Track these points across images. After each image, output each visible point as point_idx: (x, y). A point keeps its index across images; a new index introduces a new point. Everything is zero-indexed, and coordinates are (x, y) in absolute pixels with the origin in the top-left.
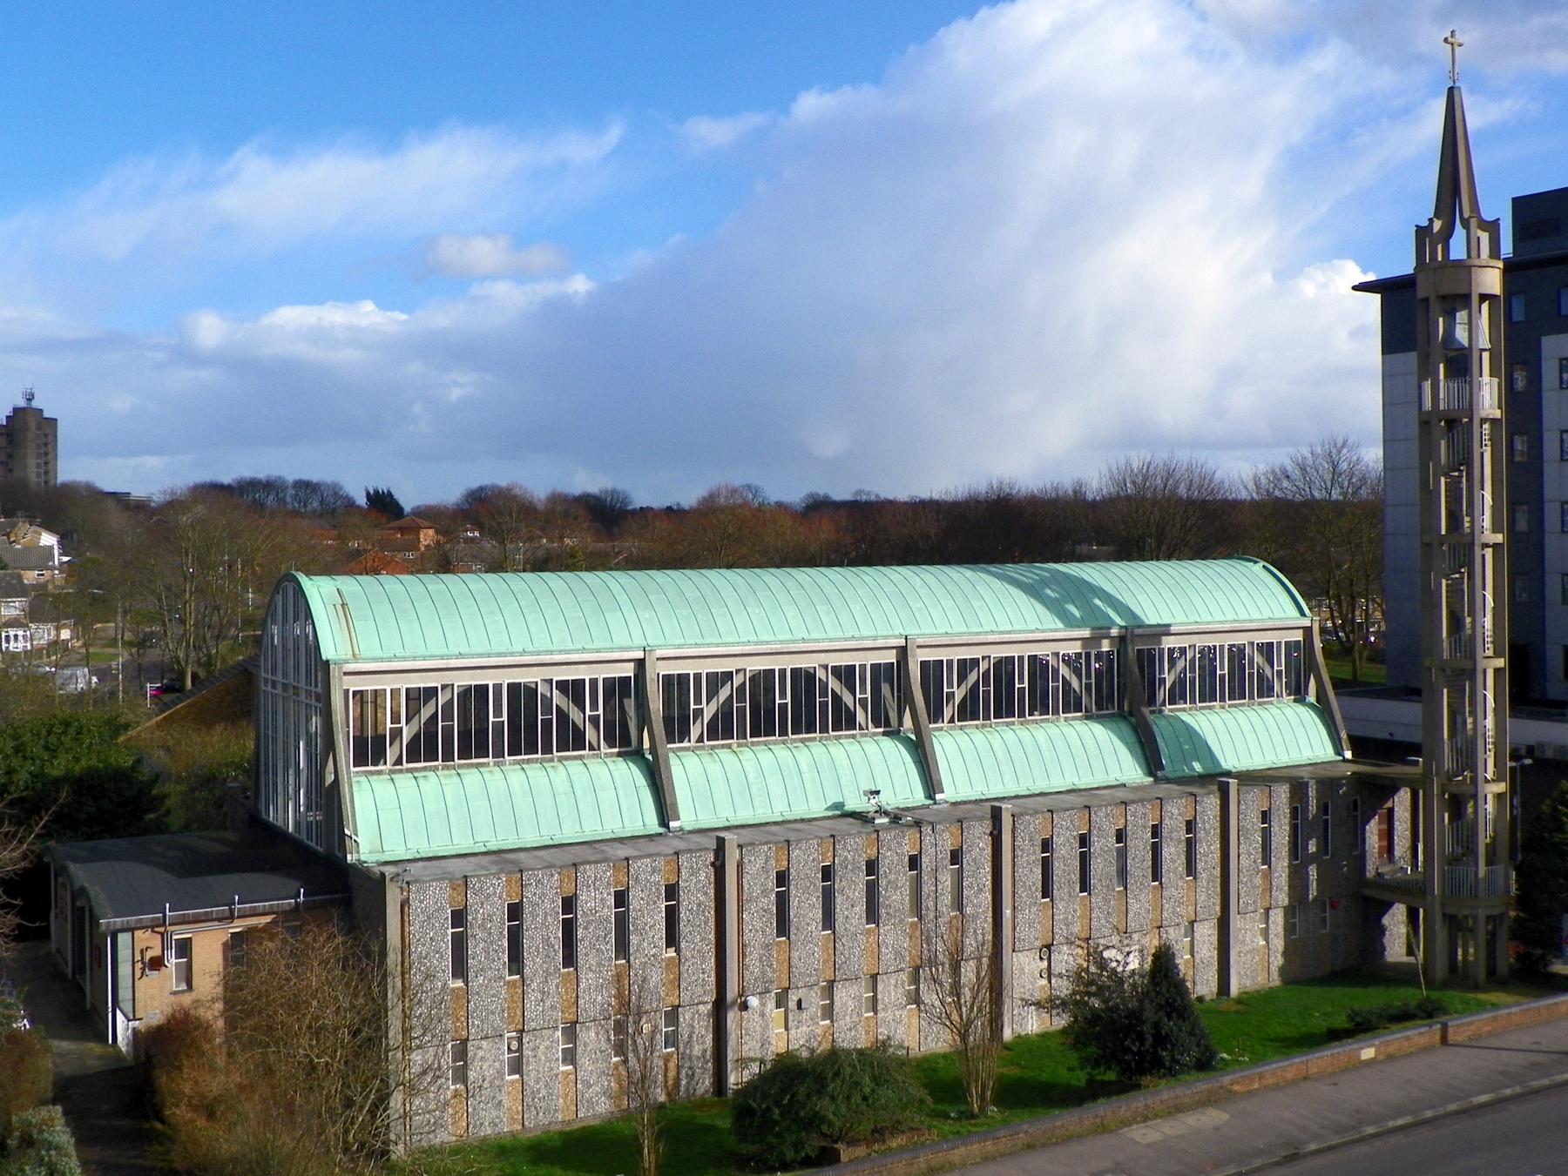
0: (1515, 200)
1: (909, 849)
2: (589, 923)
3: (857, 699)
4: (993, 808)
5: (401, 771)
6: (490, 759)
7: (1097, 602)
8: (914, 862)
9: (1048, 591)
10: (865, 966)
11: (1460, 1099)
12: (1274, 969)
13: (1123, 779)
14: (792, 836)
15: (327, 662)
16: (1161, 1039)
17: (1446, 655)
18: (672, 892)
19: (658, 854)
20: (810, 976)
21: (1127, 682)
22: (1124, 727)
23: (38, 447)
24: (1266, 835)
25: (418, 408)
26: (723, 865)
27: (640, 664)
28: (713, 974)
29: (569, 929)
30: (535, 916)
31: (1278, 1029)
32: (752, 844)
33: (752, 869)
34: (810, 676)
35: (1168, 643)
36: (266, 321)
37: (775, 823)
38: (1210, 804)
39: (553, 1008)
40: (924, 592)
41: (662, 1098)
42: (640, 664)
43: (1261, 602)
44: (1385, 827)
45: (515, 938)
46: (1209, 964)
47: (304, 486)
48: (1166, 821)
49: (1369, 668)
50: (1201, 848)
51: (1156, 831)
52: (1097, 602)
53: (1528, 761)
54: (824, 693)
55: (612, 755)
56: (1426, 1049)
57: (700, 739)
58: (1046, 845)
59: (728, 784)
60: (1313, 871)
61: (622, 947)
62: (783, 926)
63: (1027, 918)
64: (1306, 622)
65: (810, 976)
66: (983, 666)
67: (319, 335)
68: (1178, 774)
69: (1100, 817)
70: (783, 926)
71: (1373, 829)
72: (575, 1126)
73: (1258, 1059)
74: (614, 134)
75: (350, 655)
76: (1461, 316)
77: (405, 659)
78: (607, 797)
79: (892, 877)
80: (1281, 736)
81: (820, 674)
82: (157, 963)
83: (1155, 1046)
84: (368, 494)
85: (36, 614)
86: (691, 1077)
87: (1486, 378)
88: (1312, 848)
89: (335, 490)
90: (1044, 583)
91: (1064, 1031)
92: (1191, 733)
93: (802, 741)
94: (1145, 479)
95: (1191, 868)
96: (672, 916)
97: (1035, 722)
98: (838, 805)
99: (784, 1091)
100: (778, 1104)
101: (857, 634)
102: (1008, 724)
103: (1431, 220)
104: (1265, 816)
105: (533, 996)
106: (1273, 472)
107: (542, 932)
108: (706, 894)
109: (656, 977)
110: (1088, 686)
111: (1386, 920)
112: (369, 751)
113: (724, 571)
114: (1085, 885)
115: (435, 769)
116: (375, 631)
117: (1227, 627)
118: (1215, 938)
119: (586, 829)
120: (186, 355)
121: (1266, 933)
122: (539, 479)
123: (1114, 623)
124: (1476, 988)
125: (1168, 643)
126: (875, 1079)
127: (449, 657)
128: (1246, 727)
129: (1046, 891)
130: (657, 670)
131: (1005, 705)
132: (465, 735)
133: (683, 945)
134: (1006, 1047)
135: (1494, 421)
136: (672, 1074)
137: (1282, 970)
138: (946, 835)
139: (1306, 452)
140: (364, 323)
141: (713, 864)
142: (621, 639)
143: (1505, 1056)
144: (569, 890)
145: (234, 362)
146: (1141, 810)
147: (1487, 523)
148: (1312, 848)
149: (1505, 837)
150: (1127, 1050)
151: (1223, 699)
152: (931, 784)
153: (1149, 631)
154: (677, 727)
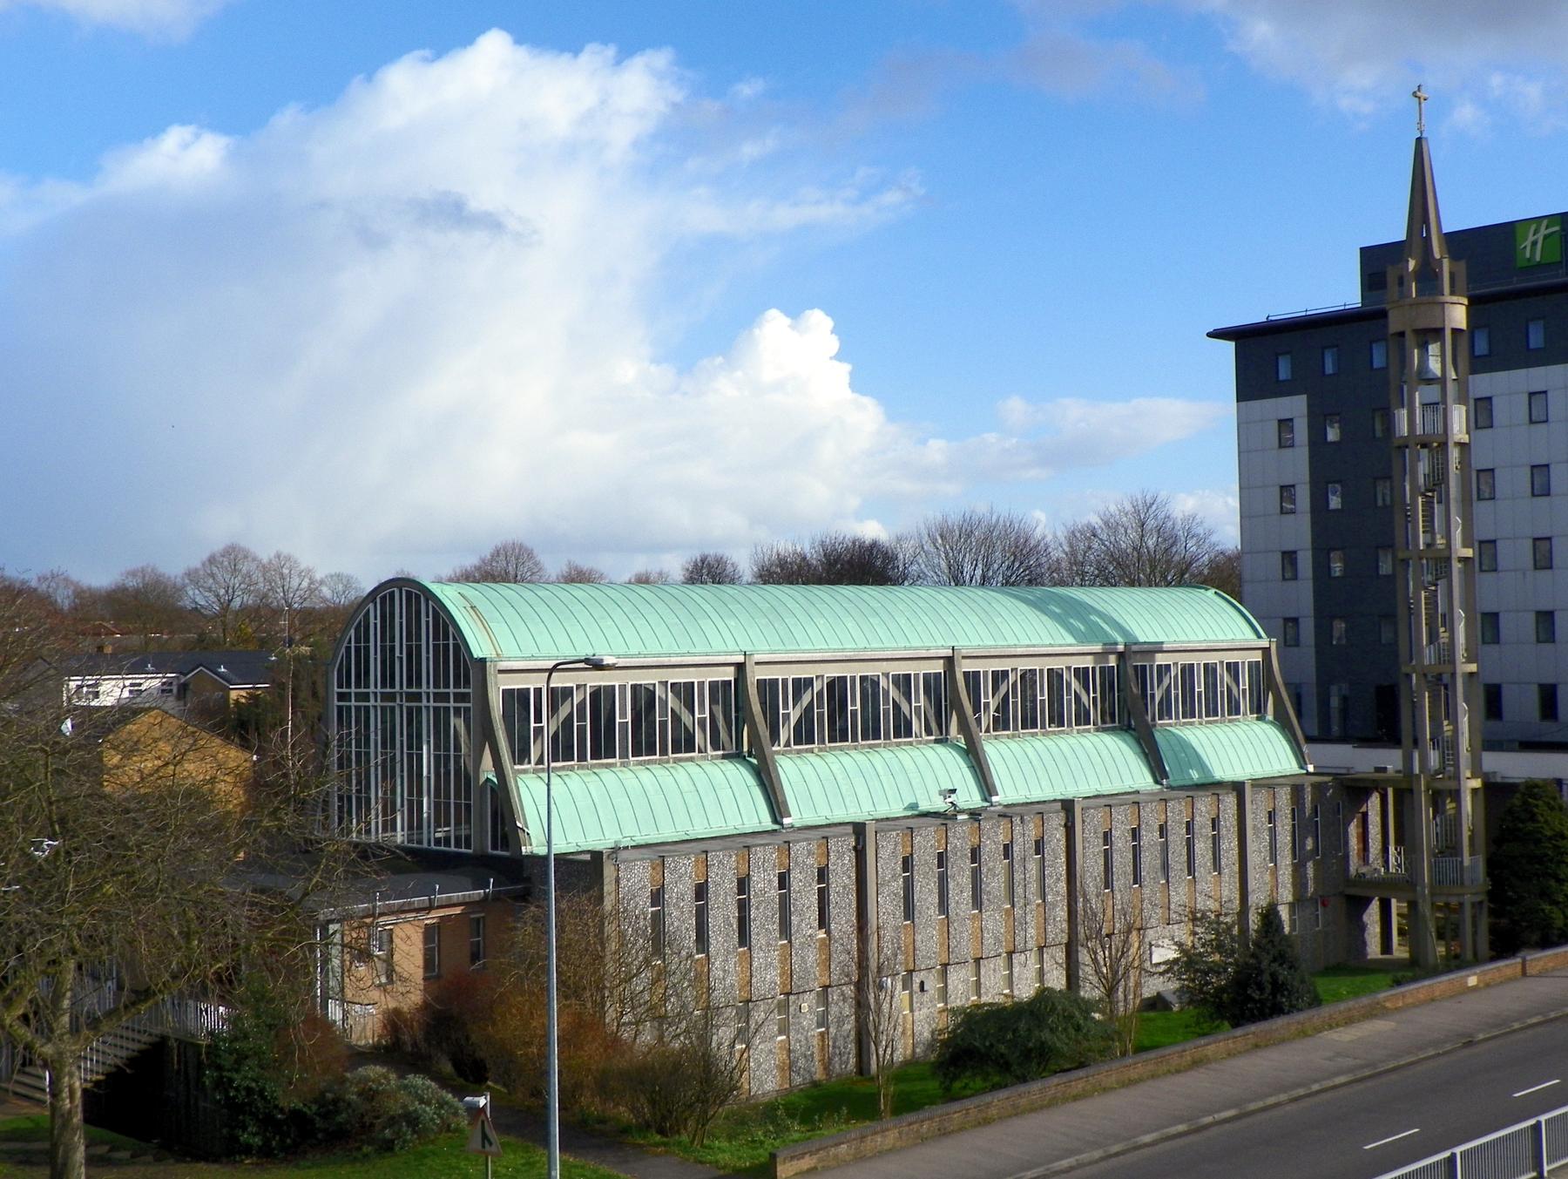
0: (1365, 252)
1: (1002, 839)
2: (760, 903)
8: (1007, 851)
13: (1136, 787)
15: (483, 661)
16: (1278, 987)
21: (1127, 695)
26: (864, 847)
27: (740, 668)
29: (743, 907)
34: (875, 683)
38: (1230, 801)
42: (740, 668)
48: (1197, 818)
55: (717, 757)
56: (1510, 980)
59: (834, 785)
62: (909, 911)
64: (1265, 643)
70: (909, 911)
71: (1353, 830)
76: (1434, 349)
81: (883, 683)
92: (1185, 746)
93: (870, 747)
98: (913, 806)
104: (1271, 816)
109: (812, 956)
115: (571, 769)
125: (1161, 659)
130: (755, 675)
139: (1113, 508)
150: (1251, 999)
152: (777, 807)
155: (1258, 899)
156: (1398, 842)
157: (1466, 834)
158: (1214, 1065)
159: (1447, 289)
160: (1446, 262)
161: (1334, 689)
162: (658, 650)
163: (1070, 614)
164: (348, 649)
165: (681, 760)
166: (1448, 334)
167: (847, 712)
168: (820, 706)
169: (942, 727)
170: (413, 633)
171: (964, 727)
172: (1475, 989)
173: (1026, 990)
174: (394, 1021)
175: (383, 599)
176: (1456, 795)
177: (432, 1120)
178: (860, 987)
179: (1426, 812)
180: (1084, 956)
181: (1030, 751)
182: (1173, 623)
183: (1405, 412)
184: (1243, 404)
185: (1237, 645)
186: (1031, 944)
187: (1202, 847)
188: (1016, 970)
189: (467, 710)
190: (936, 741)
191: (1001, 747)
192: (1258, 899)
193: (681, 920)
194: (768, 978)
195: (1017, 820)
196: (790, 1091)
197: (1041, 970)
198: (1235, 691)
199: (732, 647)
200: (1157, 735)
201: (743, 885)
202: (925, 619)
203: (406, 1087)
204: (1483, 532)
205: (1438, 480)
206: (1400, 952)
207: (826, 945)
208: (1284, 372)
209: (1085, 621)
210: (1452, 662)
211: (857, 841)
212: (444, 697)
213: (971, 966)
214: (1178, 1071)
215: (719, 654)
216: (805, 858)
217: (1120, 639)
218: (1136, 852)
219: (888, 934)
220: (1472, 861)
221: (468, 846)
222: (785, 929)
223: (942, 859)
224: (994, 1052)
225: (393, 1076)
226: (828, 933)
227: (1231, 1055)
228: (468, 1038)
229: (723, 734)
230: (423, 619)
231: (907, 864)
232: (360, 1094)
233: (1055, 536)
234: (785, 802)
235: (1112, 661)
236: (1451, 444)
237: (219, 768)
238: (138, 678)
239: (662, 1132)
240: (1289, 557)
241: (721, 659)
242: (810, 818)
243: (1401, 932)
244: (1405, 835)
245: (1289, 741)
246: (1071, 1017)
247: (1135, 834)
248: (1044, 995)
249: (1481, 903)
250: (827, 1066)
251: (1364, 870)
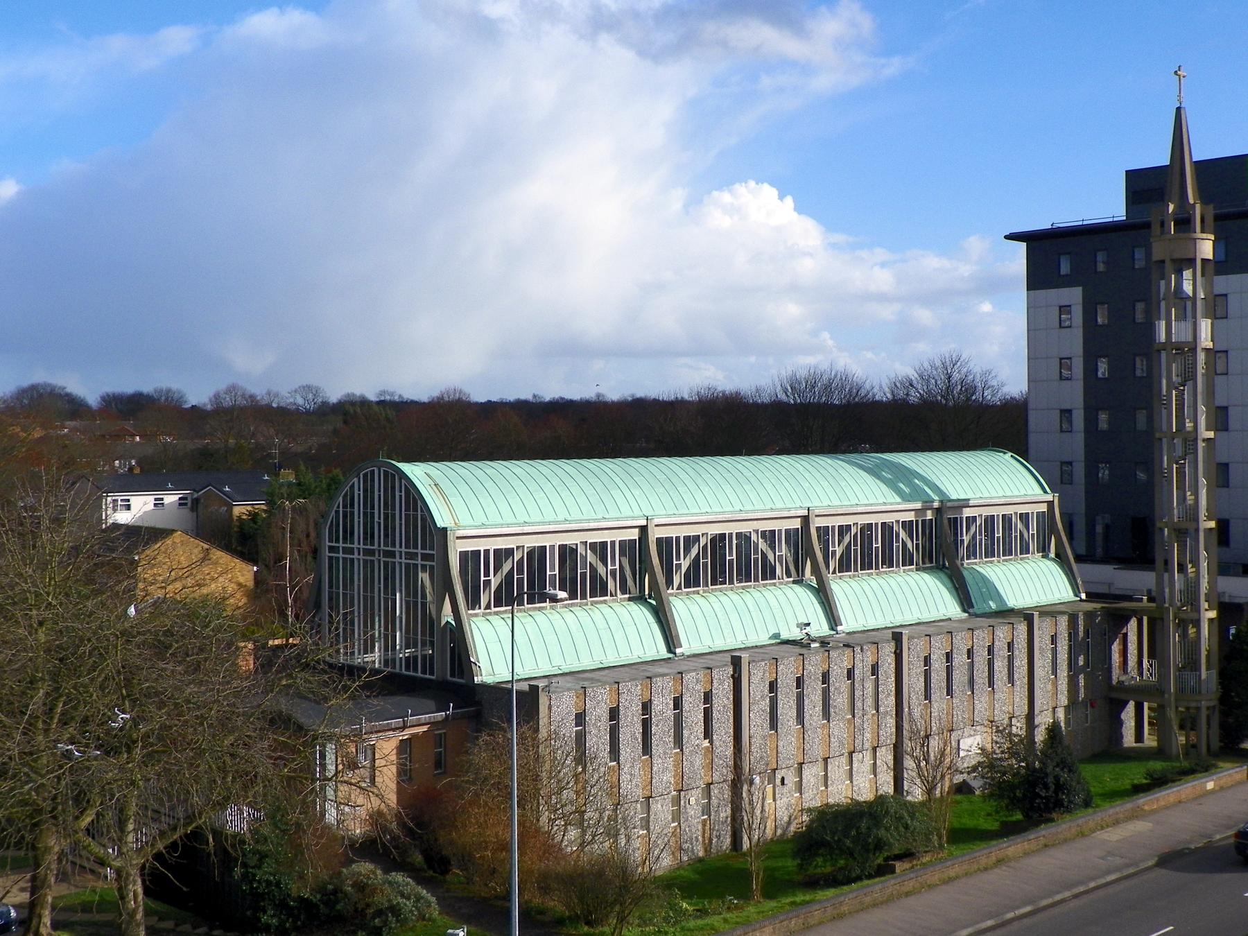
0: (1130, 174)
1: (847, 664)
2: (659, 721)
4: (733, 657)
8: (850, 674)
13: (949, 615)
14: (586, 684)
15: (445, 530)
16: (1059, 787)
21: (941, 542)
22: (942, 575)
27: (644, 530)
29: (646, 725)
30: (626, 717)
33: (755, 680)
34: (747, 538)
38: (1022, 628)
41: (701, 854)
42: (644, 530)
43: (957, 486)
48: (996, 643)
56: (1239, 783)
59: (716, 620)
62: (774, 723)
64: (1049, 497)
66: (703, 541)
70: (774, 723)
71: (1116, 647)
76: (1187, 274)
83: (1056, 792)
92: (985, 580)
93: (743, 588)
95: (1011, 679)
98: (776, 636)
104: (1054, 639)
109: (698, 761)
116: (475, 504)
117: (1002, 501)
125: (967, 513)
130: (655, 534)
131: (719, 576)
139: (926, 365)
149: (1215, 648)
152: (671, 640)
153: (956, 504)
155: (1043, 720)
156: (1151, 656)
157: (1204, 653)
158: (1013, 864)
159: (1198, 228)
160: (1198, 207)
161: (1099, 518)
162: (580, 517)
163: (899, 479)
164: (337, 512)
165: (597, 602)
166: (1199, 263)
167: (727, 561)
168: (705, 557)
169: (800, 570)
170: (389, 505)
171: (816, 571)
172: (1212, 792)
173: (865, 793)
174: (376, 818)
175: (365, 475)
176: (1197, 623)
177: (411, 911)
178: (736, 786)
179: (1175, 637)
180: (909, 763)
181: (867, 588)
182: (979, 483)
183: (1163, 323)
184: (1031, 292)
185: (1028, 499)
186: (867, 745)
187: (1000, 665)
188: (855, 766)
189: (432, 567)
190: (794, 582)
191: (844, 585)
192: (1043, 720)
193: (598, 740)
194: (665, 778)
195: (858, 649)
196: (680, 866)
197: (875, 764)
198: (1026, 535)
199: (637, 513)
200: (965, 573)
201: (646, 707)
202: (786, 484)
203: (390, 883)
204: (1220, 401)
205: (1189, 375)
206: (1150, 741)
207: (711, 750)
208: (1065, 268)
209: (911, 484)
210: (1196, 520)
211: (735, 671)
212: (412, 556)
213: (821, 764)
214: (986, 869)
215: (627, 518)
216: (694, 685)
217: (936, 498)
218: (949, 671)
219: (757, 741)
220: (1207, 674)
221: (432, 673)
222: (679, 740)
223: (799, 682)
224: (844, 847)
225: (379, 872)
226: (711, 742)
227: (1027, 854)
228: (436, 840)
229: (630, 582)
230: (397, 494)
231: (773, 687)
232: (352, 886)
233: (881, 387)
234: (678, 636)
235: (929, 515)
236: (1199, 350)
237: (230, 578)
238: (159, 495)
239: (589, 923)
240: (1066, 413)
241: (629, 523)
242: (697, 648)
243: (1150, 724)
244: (1156, 649)
245: (1066, 574)
246: (902, 818)
247: (949, 657)
248: (880, 800)
249: (1214, 707)
250: (708, 847)
251: (1123, 678)
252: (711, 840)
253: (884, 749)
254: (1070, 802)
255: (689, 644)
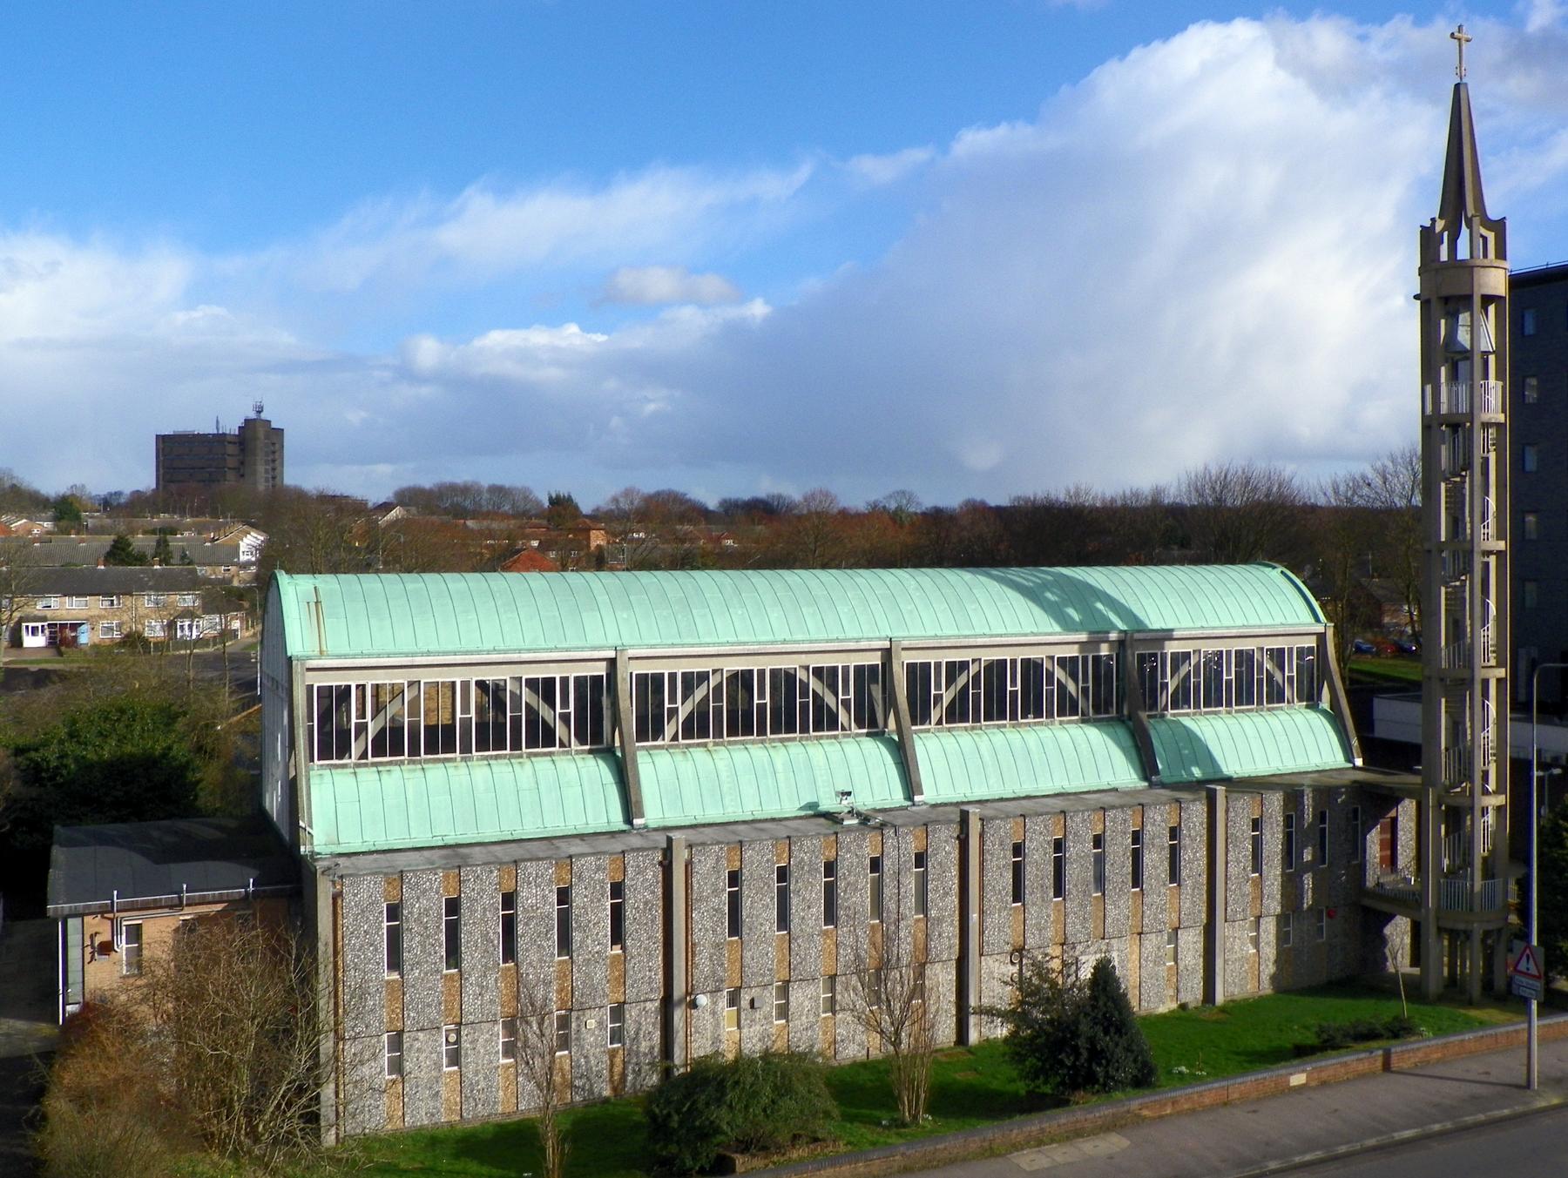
1: (869, 850)
3: (840, 701)
5: (366, 765)
6: (797, 735)
7: (1099, 606)
8: (876, 865)
9: (1049, 595)
10: (822, 967)
11: (1380, 1133)
12: (1265, 978)
13: (1114, 784)
16: (1096, 1055)
17: (1444, 665)
18: (617, 890)
19: (604, 853)
20: (763, 975)
21: (1125, 686)
22: (1121, 732)
23: (267, 454)
24: (1257, 843)
25: (616, 421)
27: (612, 663)
28: (661, 973)
29: (509, 925)
31: (1254, 1043)
32: (703, 844)
34: (790, 677)
35: (1171, 648)
36: (478, 343)
37: (744, 822)
38: (1196, 812)
39: (492, 1002)
40: (916, 595)
41: (607, 1093)
42: (612, 663)
44: (1388, 836)
45: (453, 932)
46: (1194, 971)
47: (497, 490)
48: (1148, 827)
49: (1370, 681)
50: (1186, 855)
51: (1137, 837)
52: (1099, 606)
53: (1557, 771)
54: (805, 694)
55: (583, 752)
56: (1362, 1076)
57: (675, 738)
58: (1018, 850)
59: (690, 783)
60: (1308, 881)
61: (565, 943)
63: (998, 923)
64: (1320, 629)
65: (763, 975)
66: (973, 670)
67: (525, 356)
68: (1174, 779)
69: (1075, 823)
70: (735, 927)
71: (1374, 839)
72: (516, 1118)
73: (1218, 1072)
74: (804, 172)
75: (317, 652)
76: (1464, 318)
77: (369, 656)
78: (572, 793)
79: (852, 879)
80: (1296, 742)
81: (801, 675)
82: (106, 948)
83: (1089, 1060)
84: (550, 499)
85: (210, 606)
86: (638, 1073)
87: (1492, 381)
88: (1308, 856)
89: (526, 494)
90: (1045, 586)
91: (1006, 1040)
92: (1191, 737)
93: (782, 741)
94: (1224, 487)
95: (1174, 875)
96: (617, 914)
97: (1029, 724)
99: (687, 1096)
100: (678, 1112)
101: (841, 636)
102: (999, 727)
103: (1433, 220)
104: (1256, 824)
105: (470, 990)
106: (1354, 480)
107: (482, 926)
108: (653, 892)
109: (600, 973)
110: (1085, 691)
111: (1388, 930)
112: (333, 744)
113: (819, 572)
114: (1059, 890)
116: (338, 627)
117: (1234, 632)
118: (1200, 946)
119: (941, 792)
120: (407, 373)
121: (1256, 942)
122: (709, 489)
123: (1114, 627)
124: (1470, 1004)
125: (1171, 648)
126: (775, 1088)
127: (414, 655)
128: (1250, 731)
129: (1018, 895)
130: (629, 671)
131: (742, 723)
132: (482, 727)
133: (628, 943)
134: (971, 1051)
135: (1498, 425)
136: (618, 1069)
137: (1274, 979)
138: (910, 838)
140: (563, 344)
141: (661, 863)
142: (595, 638)
143: (1447, 1087)
144: (509, 886)
145: (455, 381)
146: (1120, 815)
147: (1492, 530)
148: (1308, 856)
151: (1229, 704)
152: (910, 785)
154: (651, 726)
172: (1300, 1089)
185: (1281, 630)
251: (1388, 879)
252: (624, 1075)
253: (938, 966)
254: (1108, 1076)
255: (654, 813)
